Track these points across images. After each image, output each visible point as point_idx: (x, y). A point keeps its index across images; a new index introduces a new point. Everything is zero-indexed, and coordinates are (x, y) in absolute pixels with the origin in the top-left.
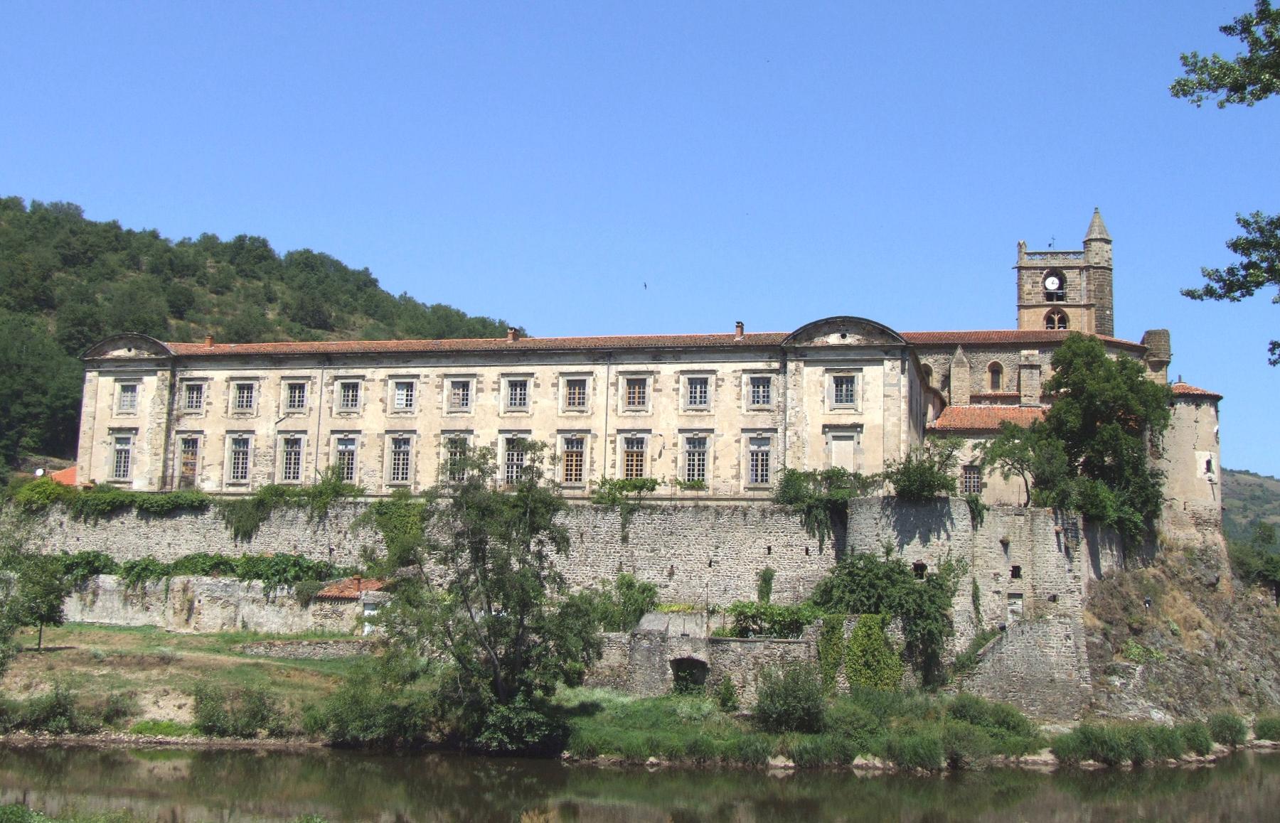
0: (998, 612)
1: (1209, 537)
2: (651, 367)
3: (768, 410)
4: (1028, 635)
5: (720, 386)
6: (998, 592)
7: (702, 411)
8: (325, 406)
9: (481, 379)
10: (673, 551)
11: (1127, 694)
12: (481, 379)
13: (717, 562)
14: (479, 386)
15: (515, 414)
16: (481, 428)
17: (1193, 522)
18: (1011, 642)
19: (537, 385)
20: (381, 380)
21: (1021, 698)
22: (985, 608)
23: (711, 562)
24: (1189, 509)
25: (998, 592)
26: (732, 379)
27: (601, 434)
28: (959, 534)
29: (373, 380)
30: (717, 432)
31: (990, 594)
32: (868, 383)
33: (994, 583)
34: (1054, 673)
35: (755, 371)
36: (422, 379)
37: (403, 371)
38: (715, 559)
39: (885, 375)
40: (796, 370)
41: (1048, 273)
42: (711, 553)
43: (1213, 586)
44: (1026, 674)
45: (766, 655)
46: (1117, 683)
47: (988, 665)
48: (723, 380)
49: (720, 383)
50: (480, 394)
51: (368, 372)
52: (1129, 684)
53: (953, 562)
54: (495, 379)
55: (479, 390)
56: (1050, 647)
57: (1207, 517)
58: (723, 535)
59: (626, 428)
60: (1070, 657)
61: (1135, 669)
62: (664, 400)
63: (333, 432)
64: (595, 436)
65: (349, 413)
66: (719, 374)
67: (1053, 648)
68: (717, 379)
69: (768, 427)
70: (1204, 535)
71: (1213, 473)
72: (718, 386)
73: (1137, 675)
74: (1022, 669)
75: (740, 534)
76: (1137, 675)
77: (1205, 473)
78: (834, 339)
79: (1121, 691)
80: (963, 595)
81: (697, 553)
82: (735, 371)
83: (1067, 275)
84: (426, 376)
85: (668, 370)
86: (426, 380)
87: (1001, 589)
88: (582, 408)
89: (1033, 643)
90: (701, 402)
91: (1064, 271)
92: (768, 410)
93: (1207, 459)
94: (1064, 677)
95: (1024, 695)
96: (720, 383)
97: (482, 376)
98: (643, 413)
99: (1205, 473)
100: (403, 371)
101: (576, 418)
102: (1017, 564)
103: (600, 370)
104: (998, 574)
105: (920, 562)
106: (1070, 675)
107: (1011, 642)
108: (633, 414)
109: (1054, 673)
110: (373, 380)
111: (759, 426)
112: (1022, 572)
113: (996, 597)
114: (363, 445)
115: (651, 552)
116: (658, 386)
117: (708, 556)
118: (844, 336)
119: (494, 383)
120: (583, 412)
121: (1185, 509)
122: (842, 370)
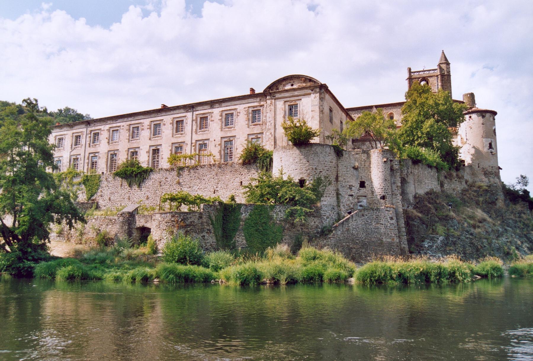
0: (352, 206)
1: (492, 180)
2: (210, 111)
3: (260, 125)
4: (366, 217)
5: (239, 116)
6: (352, 195)
7: (231, 128)
8: (88, 143)
9: (143, 125)
10: (198, 187)
11: (431, 251)
12: (143, 125)
13: (217, 191)
14: (143, 128)
15: (156, 138)
16: (143, 146)
17: (483, 173)
18: (355, 220)
19: (164, 125)
20: (107, 130)
21: (361, 252)
22: (344, 204)
23: (215, 191)
24: (481, 167)
25: (352, 195)
26: (244, 112)
27: (189, 143)
28: (326, 163)
29: (104, 130)
30: (237, 137)
31: (347, 196)
32: (304, 106)
33: (349, 190)
34: (383, 238)
35: (254, 107)
36: (122, 127)
37: (114, 125)
38: (217, 189)
39: (312, 101)
40: (271, 104)
41: (421, 80)
42: (215, 187)
43: (493, 203)
44: (365, 239)
45: (173, 221)
46: (426, 246)
47: (339, 233)
48: (240, 113)
49: (238, 114)
50: (143, 131)
51: (102, 127)
52: (433, 246)
53: (323, 178)
54: (149, 124)
55: (143, 129)
56: (381, 224)
57: (490, 170)
58: (221, 177)
59: (199, 139)
60: (393, 229)
61: (438, 239)
62: (215, 124)
63: (90, 153)
64: (187, 144)
65: (95, 145)
66: (238, 110)
67: (382, 224)
68: (237, 113)
69: (259, 132)
70: (489, 179)
71: (493, 149)
72: (238, 116)
73: (439, 242)
74: (362, 236)
75: (228, 176)
76: (439, 242)
77: (488, 149)
78: (288, 87)
79: (428, 250)
80: (329, 196)
81: (209, 187)
82: (245, 108)
83: (430, 80)
84: (123, 126)
85: (217, 111)
86: (123, 128)
87: (353, 194)
88: (182, 132)
89: (370, 222)
90: (231, 124)
91: (429, 78)
92: (260, 125)
93: (489, 142)
94: (389, 240)
95: (363, 250)
96: (238, 114)
97: (143, 123)
98: (207, 132)
99: (488, 149)
100: (114, 125)
101: (180, 137)
102: (363, 180)
103: (189, 115)
104: (352, 185)
105: (303, 179)
106: (393, 239)
107: (355, 220)
108: (202, 133)
109: (383, 238)
110: (104, 130)
111: (255, 132)
112: (366, 185)
113: (351, 198)
114: (100, 158)
115: (189, 188)
116: (212, 119)
117: (214, 188)
118: (292, 85)
119: (148, 125)
120: (182, 134)
121: (479, 167)
122: (292, 101)
